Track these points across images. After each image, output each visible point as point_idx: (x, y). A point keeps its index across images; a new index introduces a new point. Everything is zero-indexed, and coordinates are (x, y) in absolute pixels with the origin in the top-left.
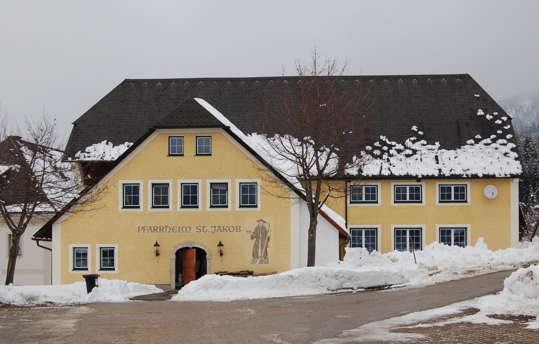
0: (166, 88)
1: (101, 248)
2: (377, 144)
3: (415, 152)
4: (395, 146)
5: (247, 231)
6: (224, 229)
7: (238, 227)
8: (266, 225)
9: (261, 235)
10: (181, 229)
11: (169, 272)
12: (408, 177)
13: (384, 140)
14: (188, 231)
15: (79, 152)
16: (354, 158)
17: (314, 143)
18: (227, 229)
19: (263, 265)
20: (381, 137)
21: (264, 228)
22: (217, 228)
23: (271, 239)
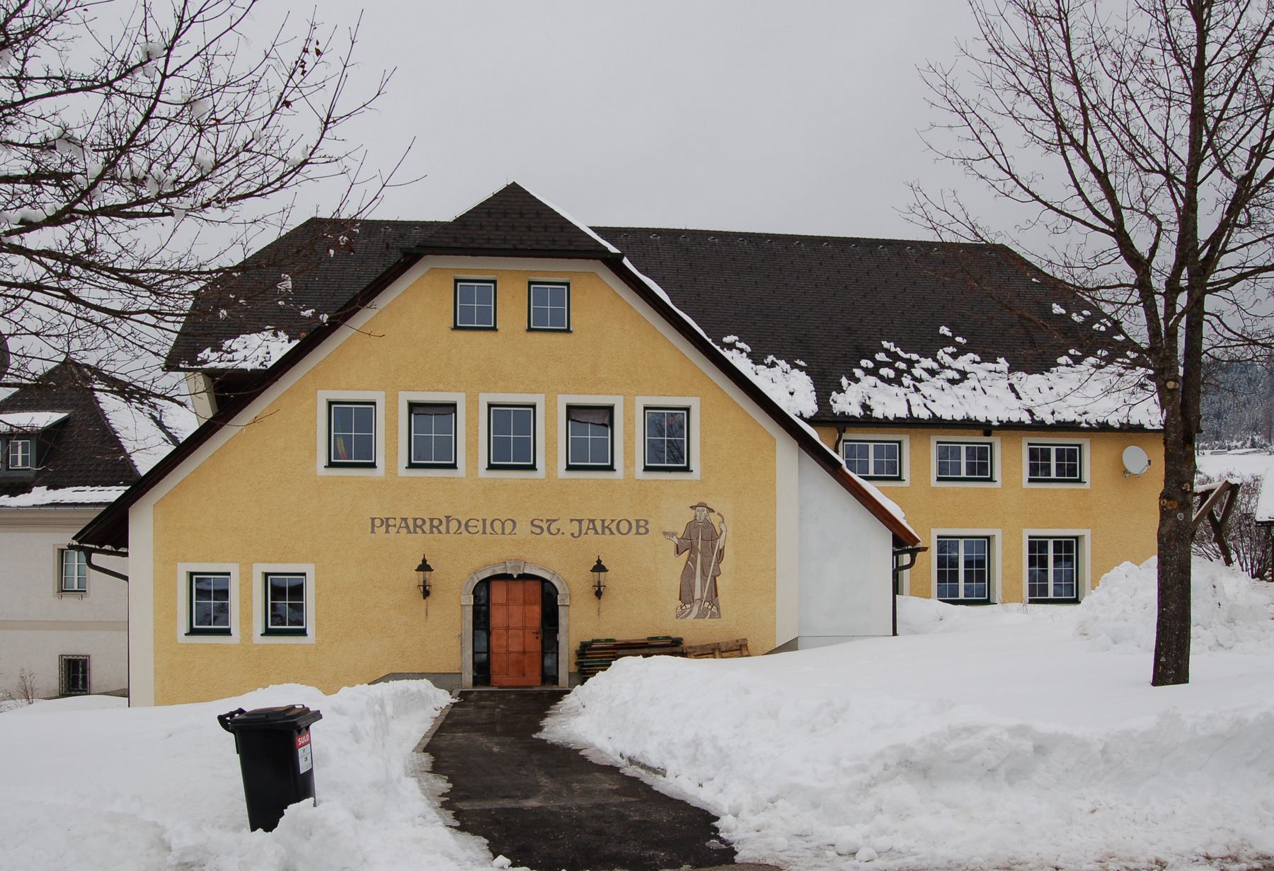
0: (401, 236)
1: (267, 575)
2: (881, 357)
3: (964, 375)
4: (918, 362)
5: (665, 533)
6: (603, 527)
7: (642, 523)
8: (714, 518)
9: (700, 543)
10: (487, 526)
11: (456, 642)
12: (968, 424)
13: (893, 349)
14: (507, 531)
15: (208, 351)
16: (844, 381)
17: (749, 350)
18: (613, 527)
19: (707, 621)
20: (886, 344)
21: (708, 525)
22: (585, 524)
23: (728, 553)
